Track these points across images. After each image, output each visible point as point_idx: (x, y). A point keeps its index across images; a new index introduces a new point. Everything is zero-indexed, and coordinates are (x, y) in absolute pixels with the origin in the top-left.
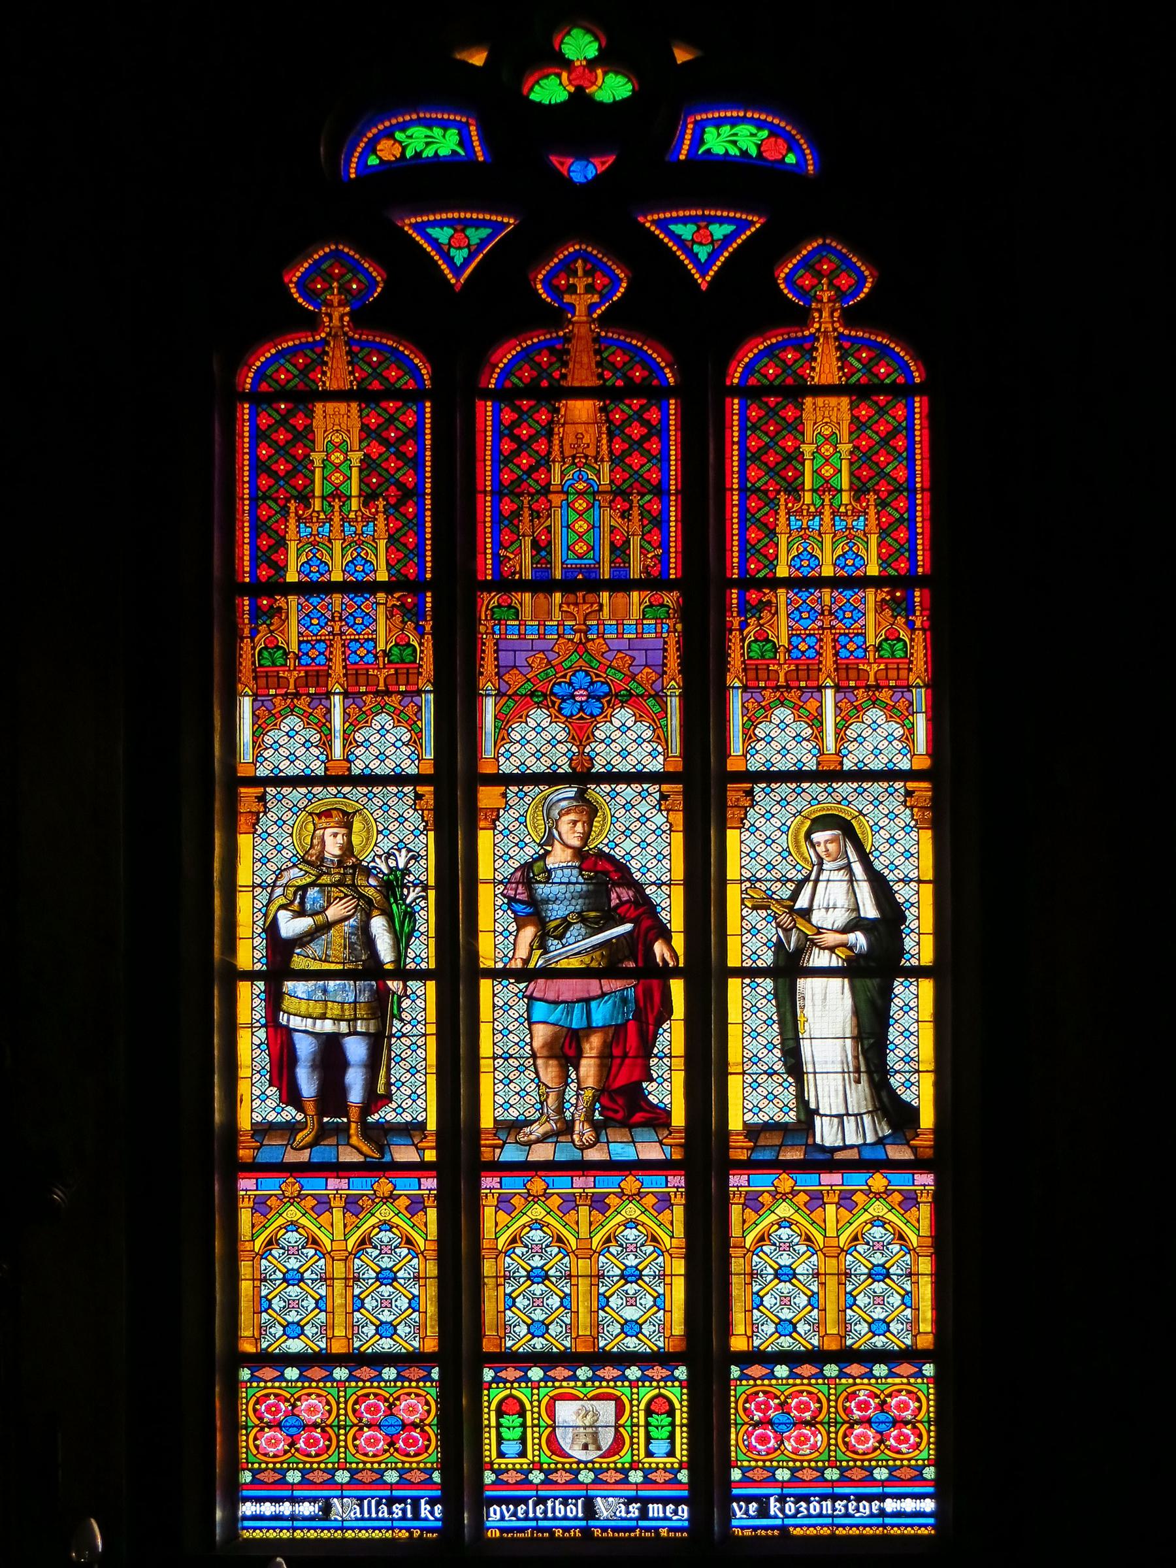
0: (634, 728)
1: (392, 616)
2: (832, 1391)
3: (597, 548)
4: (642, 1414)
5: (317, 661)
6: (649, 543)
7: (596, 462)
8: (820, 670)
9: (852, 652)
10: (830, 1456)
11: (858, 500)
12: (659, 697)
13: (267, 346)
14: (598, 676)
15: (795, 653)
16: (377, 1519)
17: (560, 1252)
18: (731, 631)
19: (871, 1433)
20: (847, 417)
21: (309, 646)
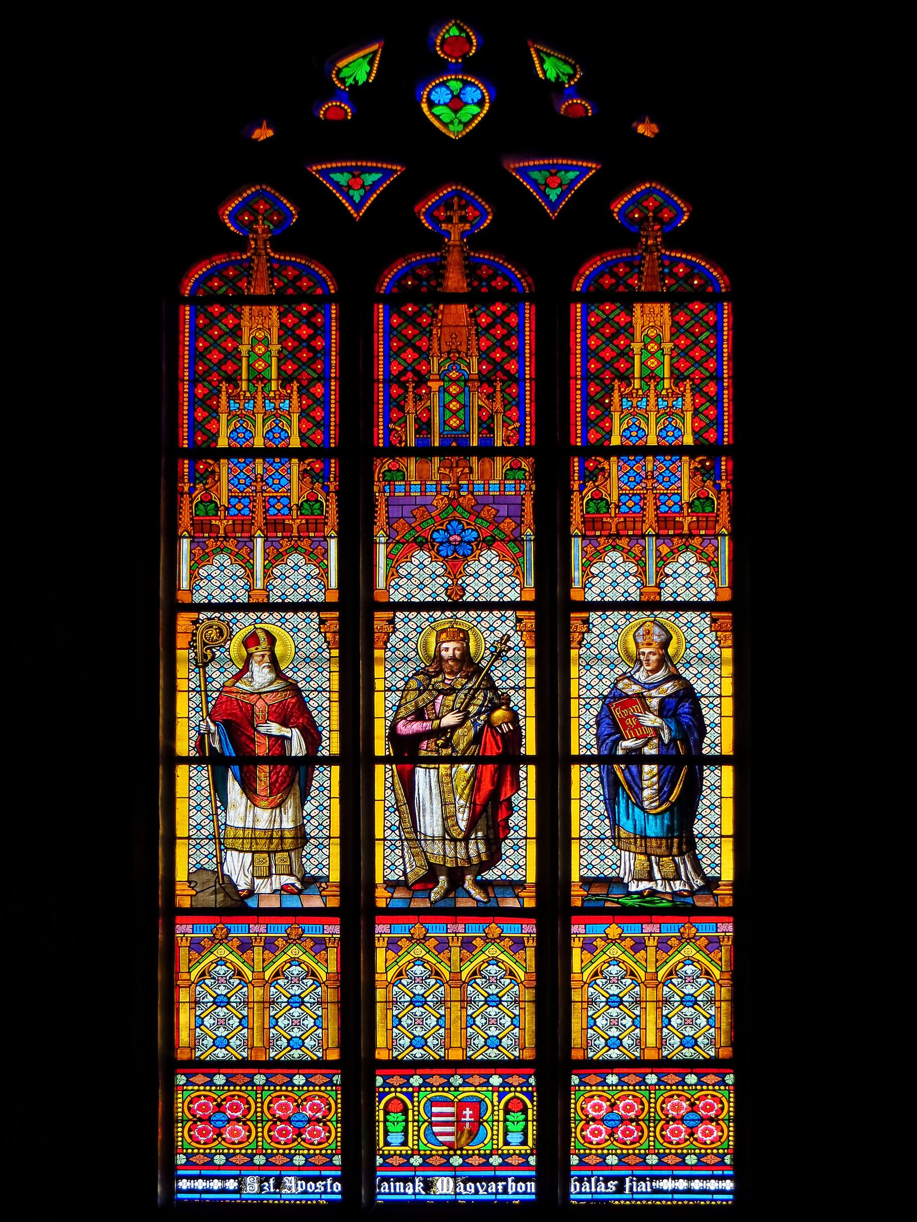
0: (497, 566)
1: (695, 476)
2: (652, 1096)
3: (467, 422)
4: (501, 1112)
5: (672, 509)
6: (510, 418)
7: (467, 356)
8: (326, 524)
9: (670, 508)
10: (649, 1146)
11: (677, 385)
12: (518, 541)
13: (204, 263)
14: (468, 524)
15: (624, 509)
16: (596, 1193)
17: (437, 982)
18: (182, 494)
19: (682, 1127)
20: (668, 322)
21: (627, 498)
